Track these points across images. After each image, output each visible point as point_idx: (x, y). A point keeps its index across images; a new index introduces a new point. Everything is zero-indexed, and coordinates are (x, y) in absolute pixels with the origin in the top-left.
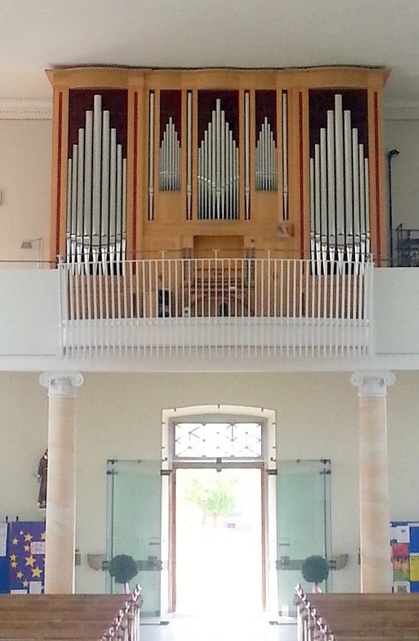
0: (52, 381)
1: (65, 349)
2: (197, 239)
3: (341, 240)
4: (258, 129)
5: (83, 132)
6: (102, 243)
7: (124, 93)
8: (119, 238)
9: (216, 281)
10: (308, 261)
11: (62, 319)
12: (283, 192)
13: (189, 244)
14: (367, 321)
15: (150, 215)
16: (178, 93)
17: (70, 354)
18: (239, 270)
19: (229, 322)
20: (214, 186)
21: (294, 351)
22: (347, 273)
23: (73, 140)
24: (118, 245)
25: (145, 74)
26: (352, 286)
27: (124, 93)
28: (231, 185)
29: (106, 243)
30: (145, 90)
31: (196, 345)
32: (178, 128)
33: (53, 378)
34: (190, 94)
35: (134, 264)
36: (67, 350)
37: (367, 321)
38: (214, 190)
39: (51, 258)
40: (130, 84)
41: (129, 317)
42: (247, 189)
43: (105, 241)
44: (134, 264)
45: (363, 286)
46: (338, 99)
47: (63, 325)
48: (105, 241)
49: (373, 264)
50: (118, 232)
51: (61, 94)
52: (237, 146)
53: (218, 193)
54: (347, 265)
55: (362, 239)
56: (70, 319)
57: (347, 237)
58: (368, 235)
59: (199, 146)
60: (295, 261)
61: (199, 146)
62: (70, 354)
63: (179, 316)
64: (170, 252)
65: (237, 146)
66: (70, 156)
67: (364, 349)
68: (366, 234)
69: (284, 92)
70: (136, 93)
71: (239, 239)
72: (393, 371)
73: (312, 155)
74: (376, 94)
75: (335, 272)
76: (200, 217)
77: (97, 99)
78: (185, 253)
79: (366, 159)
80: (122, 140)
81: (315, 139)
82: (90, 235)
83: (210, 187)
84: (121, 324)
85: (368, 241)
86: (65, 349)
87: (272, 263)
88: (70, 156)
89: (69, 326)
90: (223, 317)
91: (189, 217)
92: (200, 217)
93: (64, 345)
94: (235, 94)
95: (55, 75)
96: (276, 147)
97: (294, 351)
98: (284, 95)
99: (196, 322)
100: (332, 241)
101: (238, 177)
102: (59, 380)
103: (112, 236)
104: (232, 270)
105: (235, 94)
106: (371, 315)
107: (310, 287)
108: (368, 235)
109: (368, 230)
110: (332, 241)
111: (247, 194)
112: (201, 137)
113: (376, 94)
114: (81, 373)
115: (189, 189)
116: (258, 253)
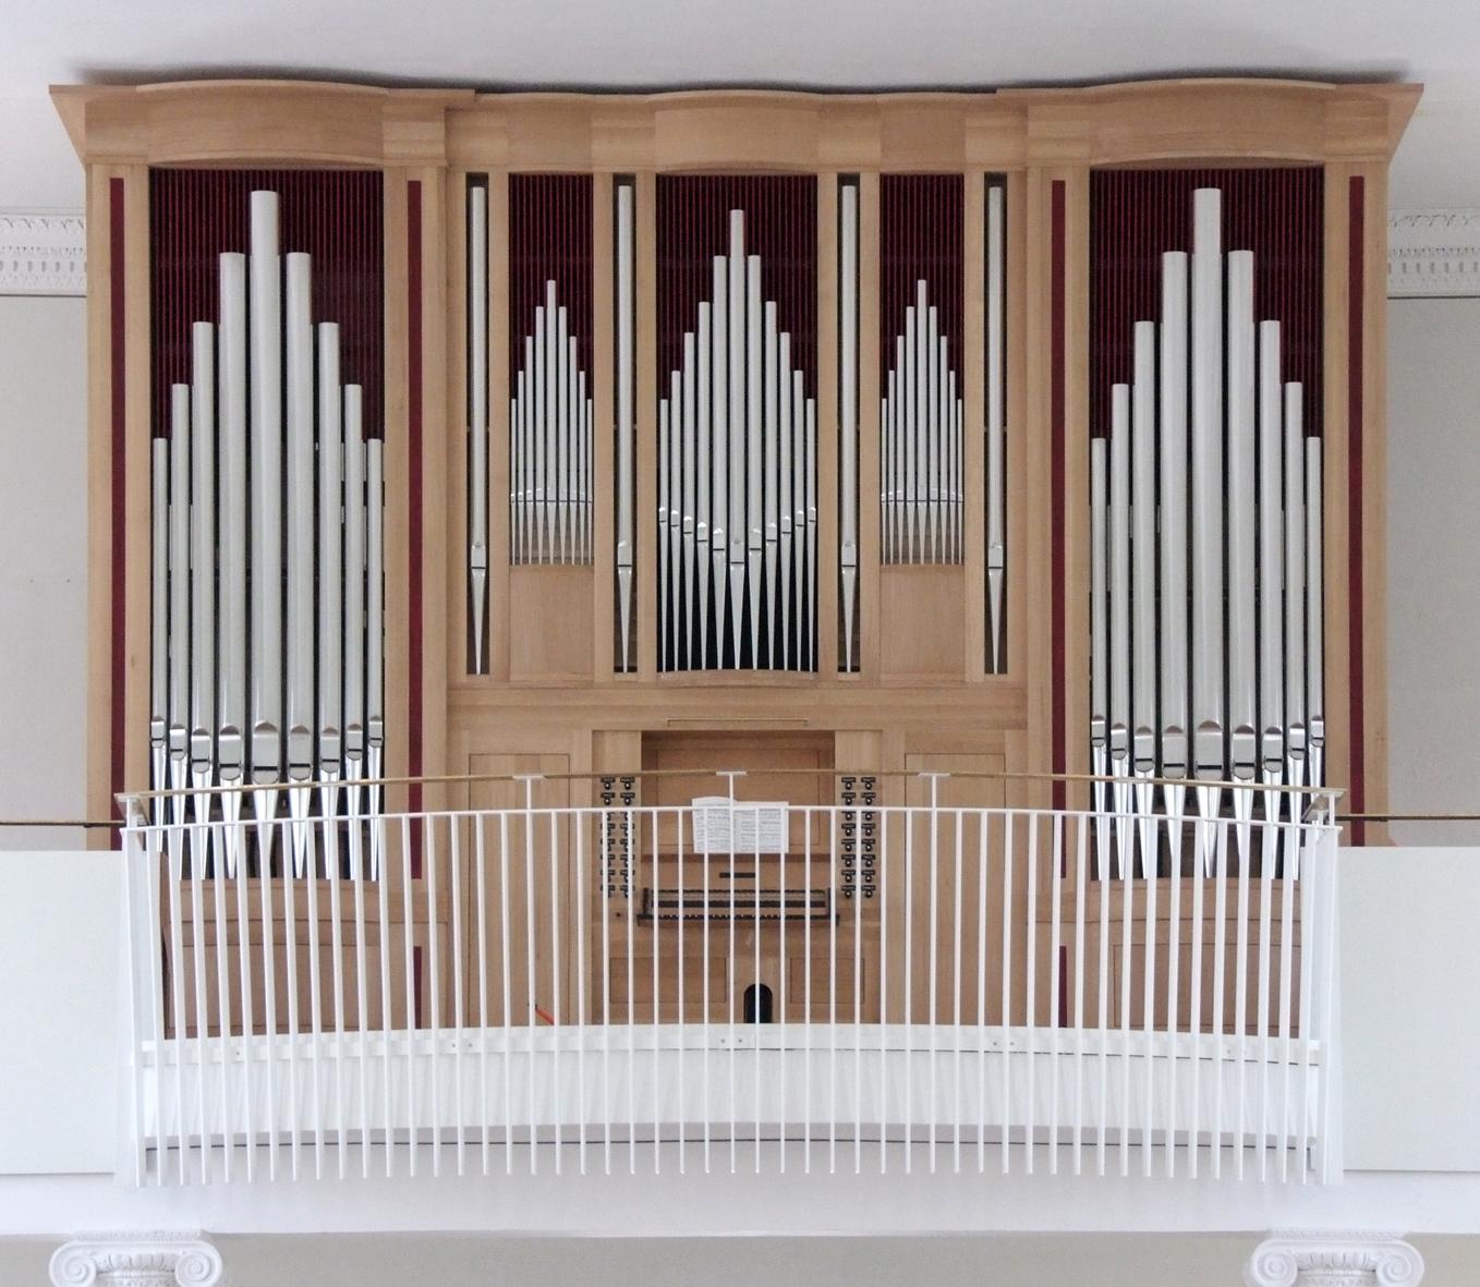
0: (99, 1272)
1: (151, 1150)
2: (655, 745)
3: (1209, 747)
4: (892, 325)
5: (667, 405)
6: (292, 759)
7: (369, 184)
8: (355, 738)
9: (808, 898)
10: (1084, 816)
11: (141, 1035)
12: (987, 568)
13: (625, 757)
14: (1313, 1045)
15: (478, 658)
16: (580, 186)
17: (172, 1167)
18: (821, 859)
19: (654, 1044)
20: (719, 542)
21: (1102, 1161)
22: (1233, 871)
23: (171, 365)
24: (354, 768)
25: (450, 112)
26: (1254, 920)
27: (369, 184)
28: (786, 540)
29: (307, 758)
30: (447, 172)
31: (225, 1131)
32: (580, 325)
33: (101, 1259)
34: (624, 191)
35: (416, 827)
36: (160, 1154)
37: (1313, 1045)
38: (719, 558)
39: (90, 811)
40: (388, 149)
41: (328, 1026)
42: (849, 556)
43: (300, 750)
44: (416, 827)
45: (1297, 922)
46: (1207, 206)
47: (143, 1060)
48: (300, 750)
49: (1335, 829)
50: (354, 716)
51: (117, 187)
52: (811, 390)
53: (737, 573)
54: (1232, 831)
55: (1292, 743)
56: (169, 1032)
57: (1235, 737)
58: (1317, 727)
59: (664, 390)
60: (1034, 814)
61: (664, 390)
62: (172, 1167)
63: (370, 1028)
64: (558, 783)
65: (811, 390)
66: (161, 424)
67: (1300, 1153)
68: (1306, 726)
69: (994, 179)
70: (414, 189)
71: (819, 746)
72: (1412, 1238)
73: (1100, 424)
74: (1357, 186)
75: (1187, 871)
76: (665, 663)
77: (263, 207)
78: (607, 788)
79: (1313, 442)
80: (361, 363)
81: (1111, 365)
82: (241, 726)
83: (703, 548)
84: (189, 1063)
85: (1316, 753)
86: (151, 1150)
87: (947, 822)
88: (161, 424)
89: (167, 1063)
90: (507, 1028)
91: (624, 662)
92: (665, 663)
93: (148, 1134)
94: (800, 190)
95: (90, 108)
96: (960, 394)
97: (1102, 1161)
98: (995, 193)
99: (480, 1046)
100: (1174, 749)
101: (812, 508)
102: (130, 1266)
103: (330, 731)
104: (826, 858)
105: (800, 190)
106: (1329, 1021)
107: (1092, 922)
108: (1317, 727)
109: (1315, 709)
110: (1174, 749)
111: (849, 576)
112: (670, 358)
113: (1357, 186)
114: (216, 1239)
115: (625, 557)
116: (886, 786)
